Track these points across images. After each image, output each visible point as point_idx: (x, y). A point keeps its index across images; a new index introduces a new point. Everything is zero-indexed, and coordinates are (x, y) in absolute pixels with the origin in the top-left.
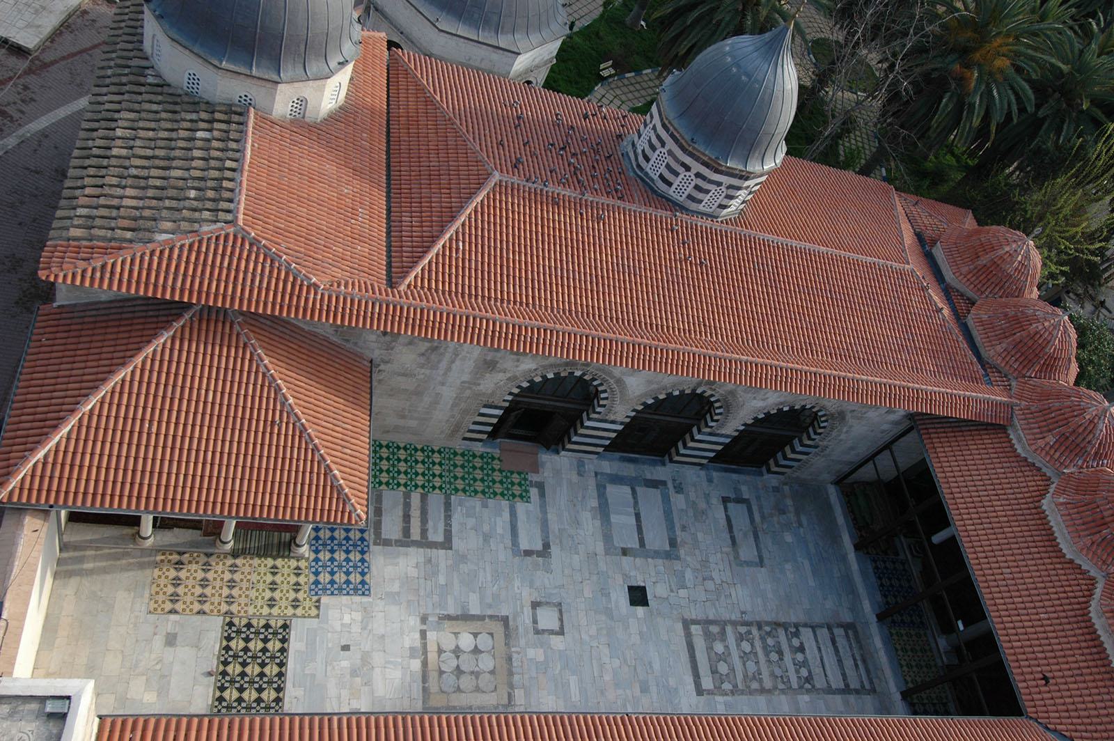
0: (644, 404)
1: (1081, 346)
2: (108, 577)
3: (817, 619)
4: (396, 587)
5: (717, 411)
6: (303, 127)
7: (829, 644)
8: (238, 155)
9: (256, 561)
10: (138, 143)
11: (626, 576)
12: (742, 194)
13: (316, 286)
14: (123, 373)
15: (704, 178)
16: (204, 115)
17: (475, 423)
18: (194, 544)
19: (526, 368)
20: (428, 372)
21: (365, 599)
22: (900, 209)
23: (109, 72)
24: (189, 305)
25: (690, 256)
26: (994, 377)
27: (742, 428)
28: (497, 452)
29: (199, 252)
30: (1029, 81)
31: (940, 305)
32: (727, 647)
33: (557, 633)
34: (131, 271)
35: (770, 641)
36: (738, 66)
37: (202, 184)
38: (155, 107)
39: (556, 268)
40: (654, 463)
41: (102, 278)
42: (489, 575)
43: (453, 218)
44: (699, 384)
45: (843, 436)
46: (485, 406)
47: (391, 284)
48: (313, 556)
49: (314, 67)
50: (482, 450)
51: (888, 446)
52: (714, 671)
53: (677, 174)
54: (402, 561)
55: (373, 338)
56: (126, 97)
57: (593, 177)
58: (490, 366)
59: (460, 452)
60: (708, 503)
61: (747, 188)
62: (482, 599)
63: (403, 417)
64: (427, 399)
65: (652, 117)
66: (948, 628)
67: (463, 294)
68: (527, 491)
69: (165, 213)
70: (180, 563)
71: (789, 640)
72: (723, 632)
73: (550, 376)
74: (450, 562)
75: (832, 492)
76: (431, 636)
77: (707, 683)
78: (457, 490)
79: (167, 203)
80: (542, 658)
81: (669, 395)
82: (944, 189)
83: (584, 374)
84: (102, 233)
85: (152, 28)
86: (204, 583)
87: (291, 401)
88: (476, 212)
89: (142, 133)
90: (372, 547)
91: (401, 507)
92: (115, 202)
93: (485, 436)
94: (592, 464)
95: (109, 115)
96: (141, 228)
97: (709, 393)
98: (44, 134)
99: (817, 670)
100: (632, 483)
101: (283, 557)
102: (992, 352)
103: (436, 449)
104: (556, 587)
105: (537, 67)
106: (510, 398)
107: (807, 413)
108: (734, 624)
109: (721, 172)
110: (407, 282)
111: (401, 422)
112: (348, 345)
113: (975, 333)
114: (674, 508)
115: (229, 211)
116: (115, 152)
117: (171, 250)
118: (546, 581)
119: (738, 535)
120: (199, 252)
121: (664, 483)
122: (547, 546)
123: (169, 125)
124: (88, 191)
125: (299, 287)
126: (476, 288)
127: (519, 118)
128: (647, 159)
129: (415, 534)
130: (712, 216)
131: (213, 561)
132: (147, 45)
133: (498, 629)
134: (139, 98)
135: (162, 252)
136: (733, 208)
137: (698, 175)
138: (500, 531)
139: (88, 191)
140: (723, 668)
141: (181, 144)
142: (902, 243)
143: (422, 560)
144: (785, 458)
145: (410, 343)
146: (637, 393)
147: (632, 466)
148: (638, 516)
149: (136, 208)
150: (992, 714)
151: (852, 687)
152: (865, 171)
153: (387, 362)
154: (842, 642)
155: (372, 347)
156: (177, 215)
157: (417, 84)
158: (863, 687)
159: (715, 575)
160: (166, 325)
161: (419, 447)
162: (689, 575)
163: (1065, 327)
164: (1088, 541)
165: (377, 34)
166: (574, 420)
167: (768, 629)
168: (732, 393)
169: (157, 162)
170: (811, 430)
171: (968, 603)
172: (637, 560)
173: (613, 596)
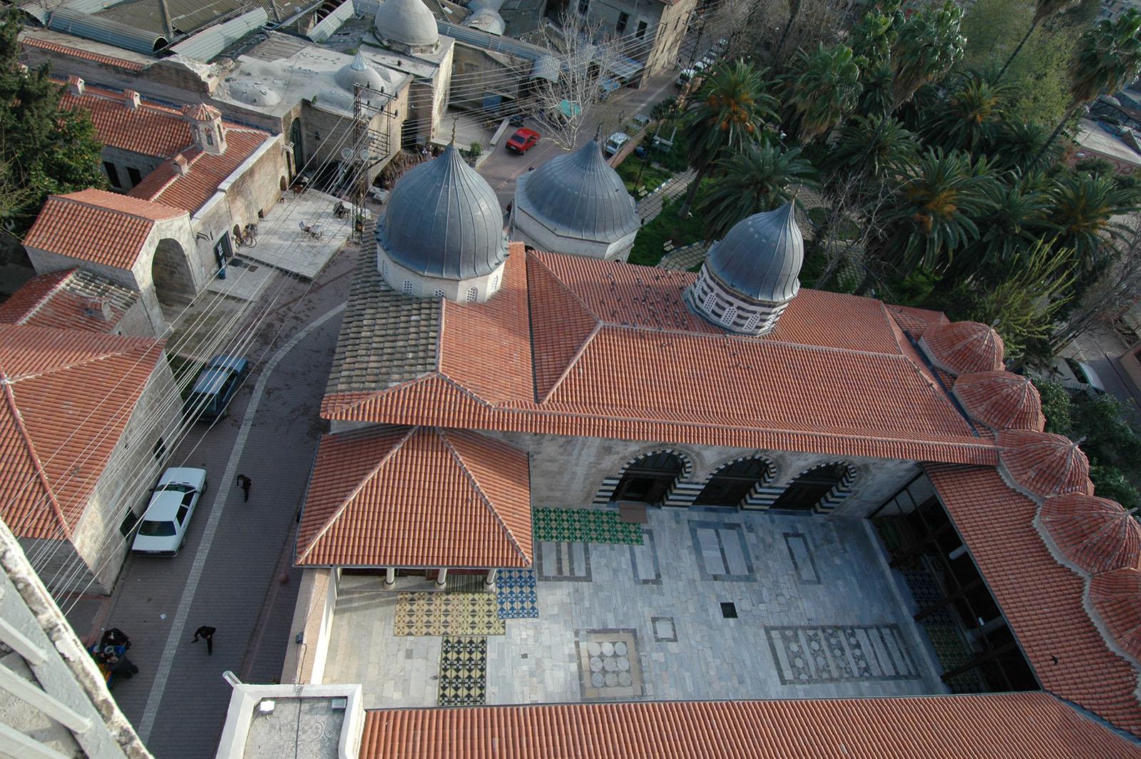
0: (718, 469)
1: (1044, 402)
3: (867, 622)
6: (475, 305)
7: (880, 641)
9: (461, 596)
10: (377, 327)
11: (718, 596)
12: (772, 317)
13: (489, 407)
16: (415, 306)
17: (600, 491)
18: (421, 586)
19: (633, 450)
20: (566, 458)
21: (535, 620)
22: (889, 316)
23: (358, 286)
24: (412, 426)
26: (980, 430)
28: (617, 510)
29: (416, 392)
30: (972, 218)
31: (930, 381)
32: (800, 646)
33: (672, 641)
34: (375, 408)
35: (833, 641)
38: (386, 304)
40: (729, 512)
41: (358, 414)
42: (619, 599)
43: (575, 354)
44: (757, 452)
45: (869, 483)
47: (538, 400)
48: (498, 591)
49: (480, 269)
50: (607, 509)
51: (905, 488)
52: (793, 666)
55: (528, 437)
56: (369, 300)
58: (608, 450)
62: (616, 617)
64: (567, 476)
66: (972, 625)
69: (394, 369)
70: (412, 600)
71: (848, 640)
72: (796, 635)
75: (867, 526)
76: (583, 645)
77: (788, 675)
78: (592, 539)
79: (395, 363)
80: (663, 660)
82: (920, 299)
85: (382, 257)
86: (429, 613)
87: (478, 484)
89: (379, 321)
92: (364, 365)
93: (608, 500)
94: (686, 514)
95: (359, 312)
96: (380, 380)
97: (764, 458)
98: (321, 328)
99: (872, 662)
100: (716, 526)
101: (479, 593)
102: (976, 412)
105: (622, 250)
106: (623, 471)
107: (839, 467)
108: (804, 628)
111: (551, 494)
113: (960, 400)
115: (433, 364)
116: (363, 334)
117: (399, 392)
119: (799, 562)
120: (416, 392)
121: (739, 525)
122: (658, 576)
123: (394, 315)
124: (347, 360)
125: (478, 407)
128: (702, 301)
129: (566, 572)
130: (753, 335)
133: (629, 638)
134: (376, 300)
135: (393, 394)
137: (739, 308)
138: (624, 566)
139: (347, 360)
140: (799, 663)
141: (402, 325)
142: (894, 340)
143: (572, 590)
144: (827, 501)
145: (552, 440)
148: (722, 551)
150: (1016, 689)
151: (901, 673)
152: (860, 293)
154: (889, 639)
155: (528, 444)
157: (545, 270)
158: (910, 673)
160: (397, 441)
162: (765, 592)
163: (1029, 389)
164: (1073, 549)
165: (518, 243)
166: (669, 484)
167: (830, 631)
169: (389, 338)
170: (844, 479)
171: (984, 603)
173: (711, 611)
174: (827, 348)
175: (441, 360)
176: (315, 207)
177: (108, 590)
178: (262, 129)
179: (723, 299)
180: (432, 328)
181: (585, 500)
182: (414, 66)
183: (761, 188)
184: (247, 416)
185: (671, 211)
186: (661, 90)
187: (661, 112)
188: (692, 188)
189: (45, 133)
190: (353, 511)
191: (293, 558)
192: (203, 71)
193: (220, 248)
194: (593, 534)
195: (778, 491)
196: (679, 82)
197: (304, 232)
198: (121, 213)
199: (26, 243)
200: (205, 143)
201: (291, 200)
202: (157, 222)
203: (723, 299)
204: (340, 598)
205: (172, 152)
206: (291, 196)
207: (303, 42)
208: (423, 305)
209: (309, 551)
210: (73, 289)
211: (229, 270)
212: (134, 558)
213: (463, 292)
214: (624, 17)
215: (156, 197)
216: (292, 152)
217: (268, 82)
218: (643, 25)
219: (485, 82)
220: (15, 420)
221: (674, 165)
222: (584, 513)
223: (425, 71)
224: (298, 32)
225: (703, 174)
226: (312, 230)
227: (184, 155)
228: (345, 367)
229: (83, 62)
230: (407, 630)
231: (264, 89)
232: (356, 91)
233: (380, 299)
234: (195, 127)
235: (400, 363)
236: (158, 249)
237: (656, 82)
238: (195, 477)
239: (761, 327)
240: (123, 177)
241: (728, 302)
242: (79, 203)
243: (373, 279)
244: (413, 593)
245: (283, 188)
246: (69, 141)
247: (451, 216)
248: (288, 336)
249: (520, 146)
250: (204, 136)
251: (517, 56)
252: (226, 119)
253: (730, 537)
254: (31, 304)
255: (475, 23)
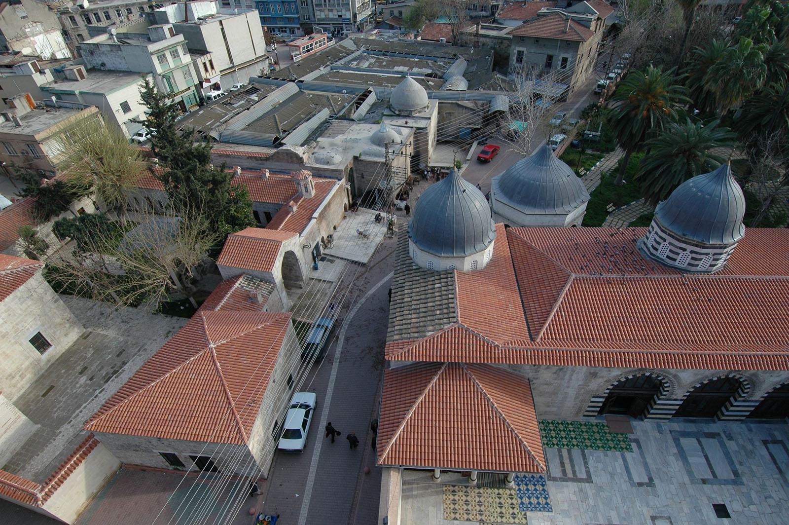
0: (694, 387)
2: (424, 499)
4: (565, 506)
5: (746, 387)
6: (477, 273)
8: (453, 291)
9: (489, 491)
10: (414, 294)
11: (709, 498)
12: (724, 256)
13: (498, 346)
14: (421, 398)
15: (697, 253)
16: (437, 277)
18: (459, 481)
19: (616, 374)
21: (550, 514)
23: (399, 268)
24: (444, 363)
25: (700, 297)
27: (766, 395)
28: (605, 422)
34: (419, 351)
36: (701, 191)
37: (441, 307)
38: (418, 278)
39: (619, 317)
40: (707, 422)
42: (619, 499)
43: (556, 301)
44: (731, 372)
46: (593, 397)
48: (517, 488)
49: (478, 247)
53: (678, 254)
54: (565, 490)
57: (626, 265)
58: (594, 375)
59: (583, 423)
60: (753, 445)
61: (726, 253)
63: (549, 406)
65: (653, 228)
67: (571, 339)
68: (630, 445)
70: (454, 491)
73: (630, 377)
74: (594, 491)
78: (587, 446)
79: (429, 318)
81: (711, 381)
83: (651, 374)
84: (406, 336)
85: (413, 247)
86: (467, 503)
87: (496, 405)
88: (567, 295)
90: (548, 482)
91: (558, 457)
92: (409, 321)
93: (596, 414)
94: (666, 426)
95: (401, 285)
97: (738, 376)
98: (374, 295)
100: (697, 436)
101: (502, 488)
103: (569, 422)
104: (664, 507)
105: (577, 218)
106: (608, 391)
109: (707, 248)
110: (540, 337)
111: (548, 409)
112: (516, 372)
114: (730, 451)
115: (454, 317)
116: (406, 300)
118: (657, 503)
121: (718, 434)
123: (424, 285)
124: (398, 318)
125: (490, 348)
126: (577, 335)
127: (576, 244)
128: (656, 250)
130: (707, 272)
131: (469, 490)
132: (411, 254)
136: (720, 265)
137: (692, 252)
138: (619, 471)
139: (398, 318)
141: (430, 291)
143: (577, 489)
145: (548, 368)
146: (689, 381)
147: (692, 425)
149: (417, 323)
153: (537, 379)
156: (433, 323)
159: (773, 494)
160: (435, 373)
161: (560, 422)
162: (754, 495)
166: (649, 401)
168: (755, 375)
172: (714, 486)
173: (704, 511)
174: (781, 277)
175: (459, 314)
176: (365, 217)
177: (266, 477)
178: (333, 178)
179: (676, 247)
180: (450, 292)
181: (577, 413)
182: (415, 122)
183: (689, 155)
184: (336, 356)
185: (607, 181)
186: (584, 98)
187: (587, 114)
188: (622, 163)
189: (225, 200)
190: (411, 426)
191: (374, 459)
192: (300, 151)
193: (315, 252)
194: (588, 443)
195: (753, 404)
196: (597, 90)
197: (357, 235)
198: (265, 240)
199: (217, 263)
200: (304, 191)
201: (350, 217)
202: (283, 243)
203: (676, 247)
204: (404, 487)
205: (287, 200)
206: (350, 214)
207: (350, 122)
208: (442, 276)
209: (385, 455)
210: (242, 286)
211: (320, 264)
212: (280, 454)
213: (467, 264)
214: (550, 58)
215: (281, 227)
216: (349, 188)
217: (334, 150)
218: (565, 60)
219: (461, 122)
220: (217, 369)
221: (603, 147)
222: (577, 425)
223: (422, 124)
224: (346, 118)
225: (638, 156)
226: (364, 233)
227: (294, 200)
228: (397, 323)
229: (238, 157)
230: (453, 516)
231: (333, 154)
232: (386, 146)
233: (414, 275)
234: (299, 184)
235: (431, 318)
236: (284, 258)
237: (580, 94)
238: (310, 398)
239: (714, 265)
240: (262, 217)
241: (680, 248)
242: (243, 237)
243: (408, 261)
244: (454, 486)
245: (346, 210)
246: (236, 203)
247: (457, 215)
248: (355, 302)
249: (487, 157)
250: (303, 188)
251: (479, 100)
252: (314, 176)
253: (712, 446)
254: (222, 297)
255: (448, 86)
